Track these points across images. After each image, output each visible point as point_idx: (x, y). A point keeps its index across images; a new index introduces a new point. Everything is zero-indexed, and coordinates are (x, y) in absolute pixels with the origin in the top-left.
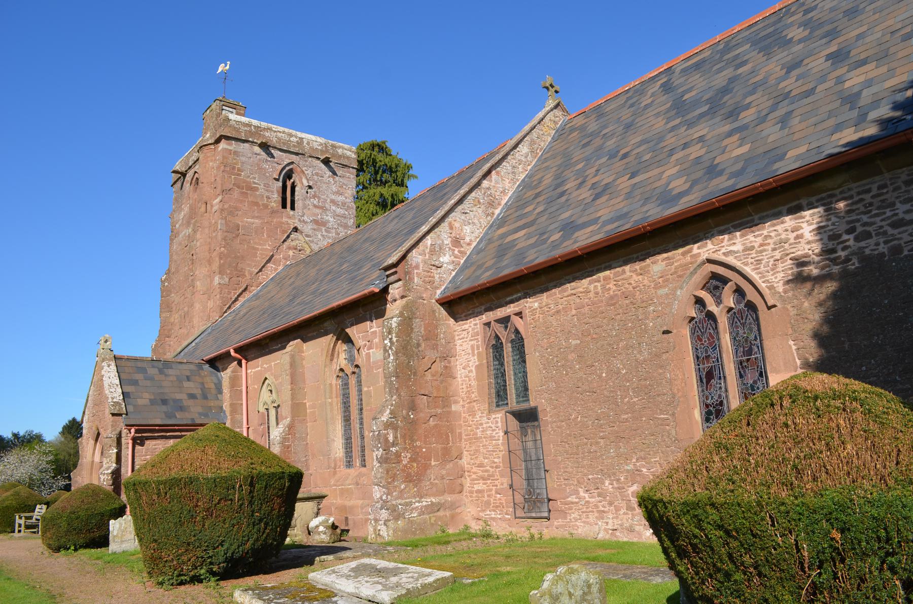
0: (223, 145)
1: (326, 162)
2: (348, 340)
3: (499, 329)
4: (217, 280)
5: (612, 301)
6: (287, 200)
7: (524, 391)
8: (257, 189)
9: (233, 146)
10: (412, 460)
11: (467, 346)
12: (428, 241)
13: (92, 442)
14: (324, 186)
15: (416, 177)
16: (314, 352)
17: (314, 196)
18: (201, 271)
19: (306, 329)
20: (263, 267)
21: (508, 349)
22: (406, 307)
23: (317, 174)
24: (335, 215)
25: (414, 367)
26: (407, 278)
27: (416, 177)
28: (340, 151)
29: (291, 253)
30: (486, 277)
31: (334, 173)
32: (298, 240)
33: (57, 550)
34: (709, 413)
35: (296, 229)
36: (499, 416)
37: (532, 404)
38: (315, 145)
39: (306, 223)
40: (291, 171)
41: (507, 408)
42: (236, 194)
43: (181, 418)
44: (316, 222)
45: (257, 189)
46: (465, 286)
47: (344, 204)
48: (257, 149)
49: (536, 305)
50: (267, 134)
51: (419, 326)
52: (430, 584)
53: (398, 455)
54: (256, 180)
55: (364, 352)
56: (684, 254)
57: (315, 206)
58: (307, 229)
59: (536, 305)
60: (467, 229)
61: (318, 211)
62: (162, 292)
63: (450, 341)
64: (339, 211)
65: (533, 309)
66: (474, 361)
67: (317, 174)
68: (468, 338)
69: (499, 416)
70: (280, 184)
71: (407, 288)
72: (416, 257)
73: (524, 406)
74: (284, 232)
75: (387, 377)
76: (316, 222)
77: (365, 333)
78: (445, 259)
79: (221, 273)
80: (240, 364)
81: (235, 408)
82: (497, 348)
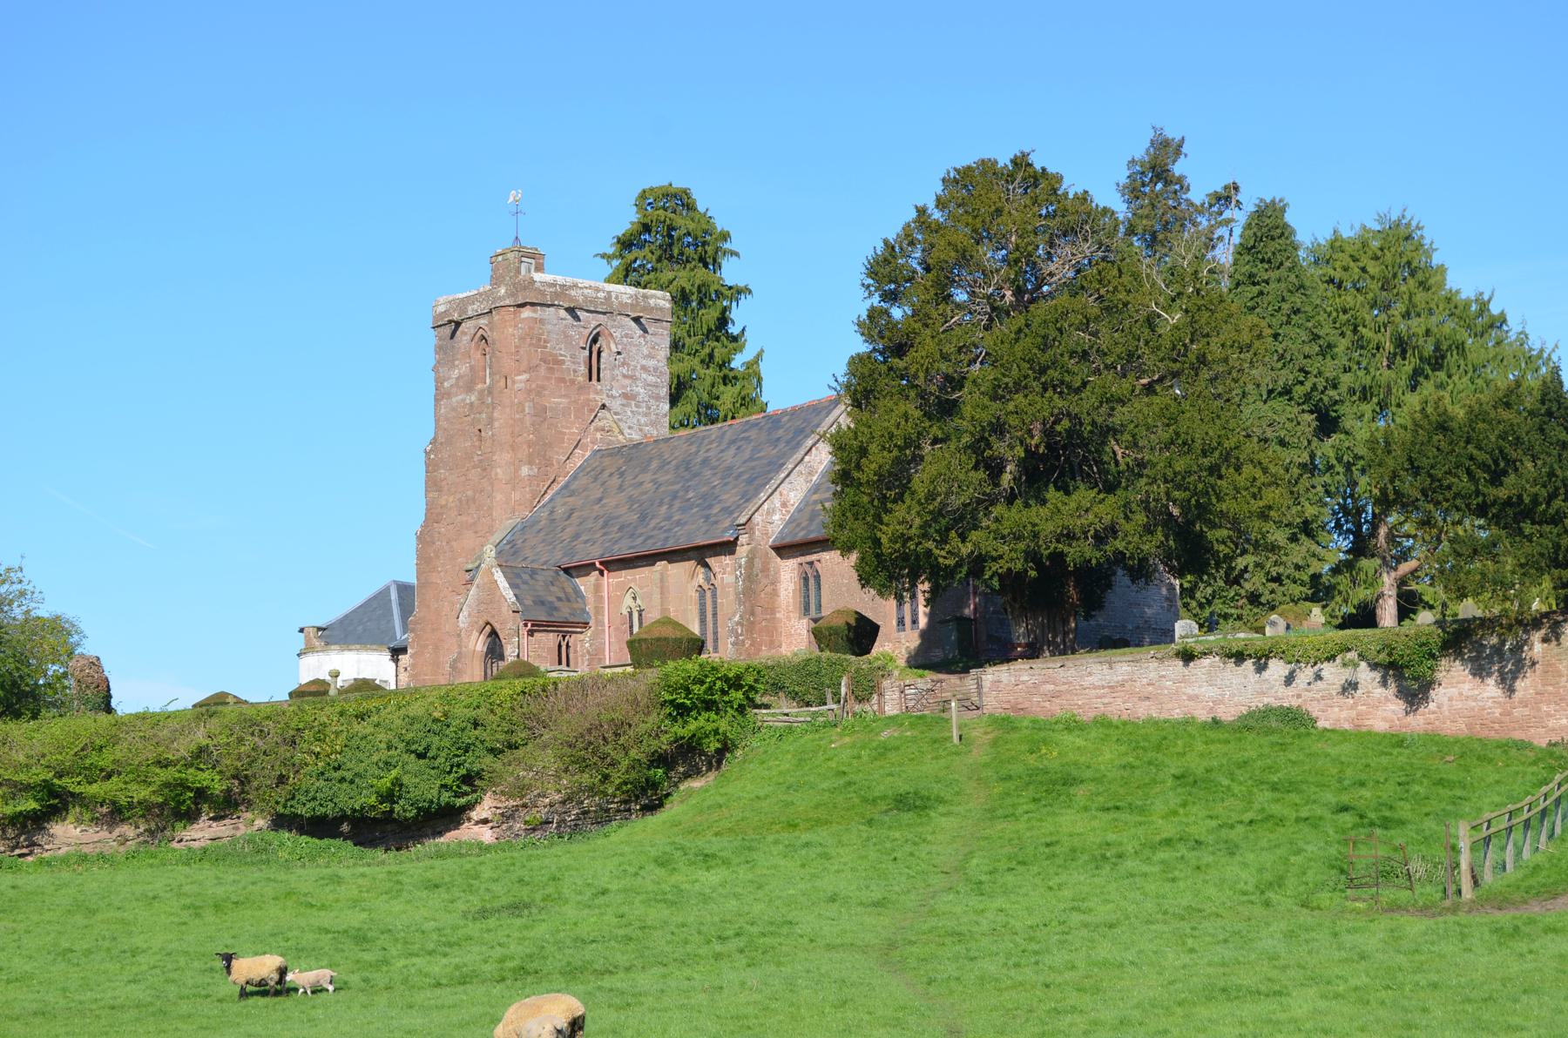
0: (526, 313)
1: (637, 320)
2: (706, 566)
3: (807, 568)
4: (525, 470)
6: (594, 372)
7: (819, 607)
8: (563, 362)
9: (540, 313)
11: (788, 576)
12: (766, 506)
14: (634, 349)
15: (737, 254)
16: (678, 572)
17: (623, 364)
18: (503, 457)
19: (673, 556)
21: (812, 581)
22: (751, 551)
23: (627, 336)
24: (647, 385)
25: (754, 589)
26: (751, 532)
27: (737, 254)
28: (652, 302)
29: (598, 435)
30: (800, 536)
31: (645, 331)
32: (606, 419)
35: (603, 406)
36: (805, 621)
38: (625, 299)
39: (613, 397)
40: (598, 334)
42: (543, 371)
43: (557, 617)
44: (625, 396)
45: (563, 362)
46: (788, 540)
47: (656, 369)
48: (563, 313)
50: (573, 293)
51: (758, 564)
52: (807, 437)
54: (563, 352)
55: (719, 576)
57: (625, 376)
58: (615, 405)
60: (792, 494)
61: (627, 382)
62: (427, 465)
63: (777, 572)
64: (651, 379)
66: (792, 587)
67: (627, 336)
68: (788, 571)
69: (805, 621)
70: (587, 353)
71: (751, 539)
72: (757, 518)
74: (592, 410)
75: (737, 594)
76: (625, 396)
77: (722, 565)
78: (776, 517)
79: (530, 463)
80: (602, 573)
82: (806, 579)
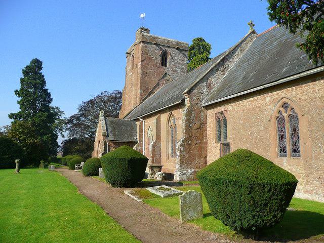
5: (254, 109)
6: (164, 63)
10: (189, 157)
13: (98, 144)
20: (246, 39)
21: (222, 123)
33: (87, 176)
34: (281, 150)
36: (219, 144)
37: (228, 141)
41: (221, 142)
49: (231, 108)
51: (194, 114)
53: (184, 155)
56: (277, 94)
59: (231, 108)
65: (230, 108)
69: (219, 144)
73: (226, 142)
81: (141, 136)
82: (219, 122)
